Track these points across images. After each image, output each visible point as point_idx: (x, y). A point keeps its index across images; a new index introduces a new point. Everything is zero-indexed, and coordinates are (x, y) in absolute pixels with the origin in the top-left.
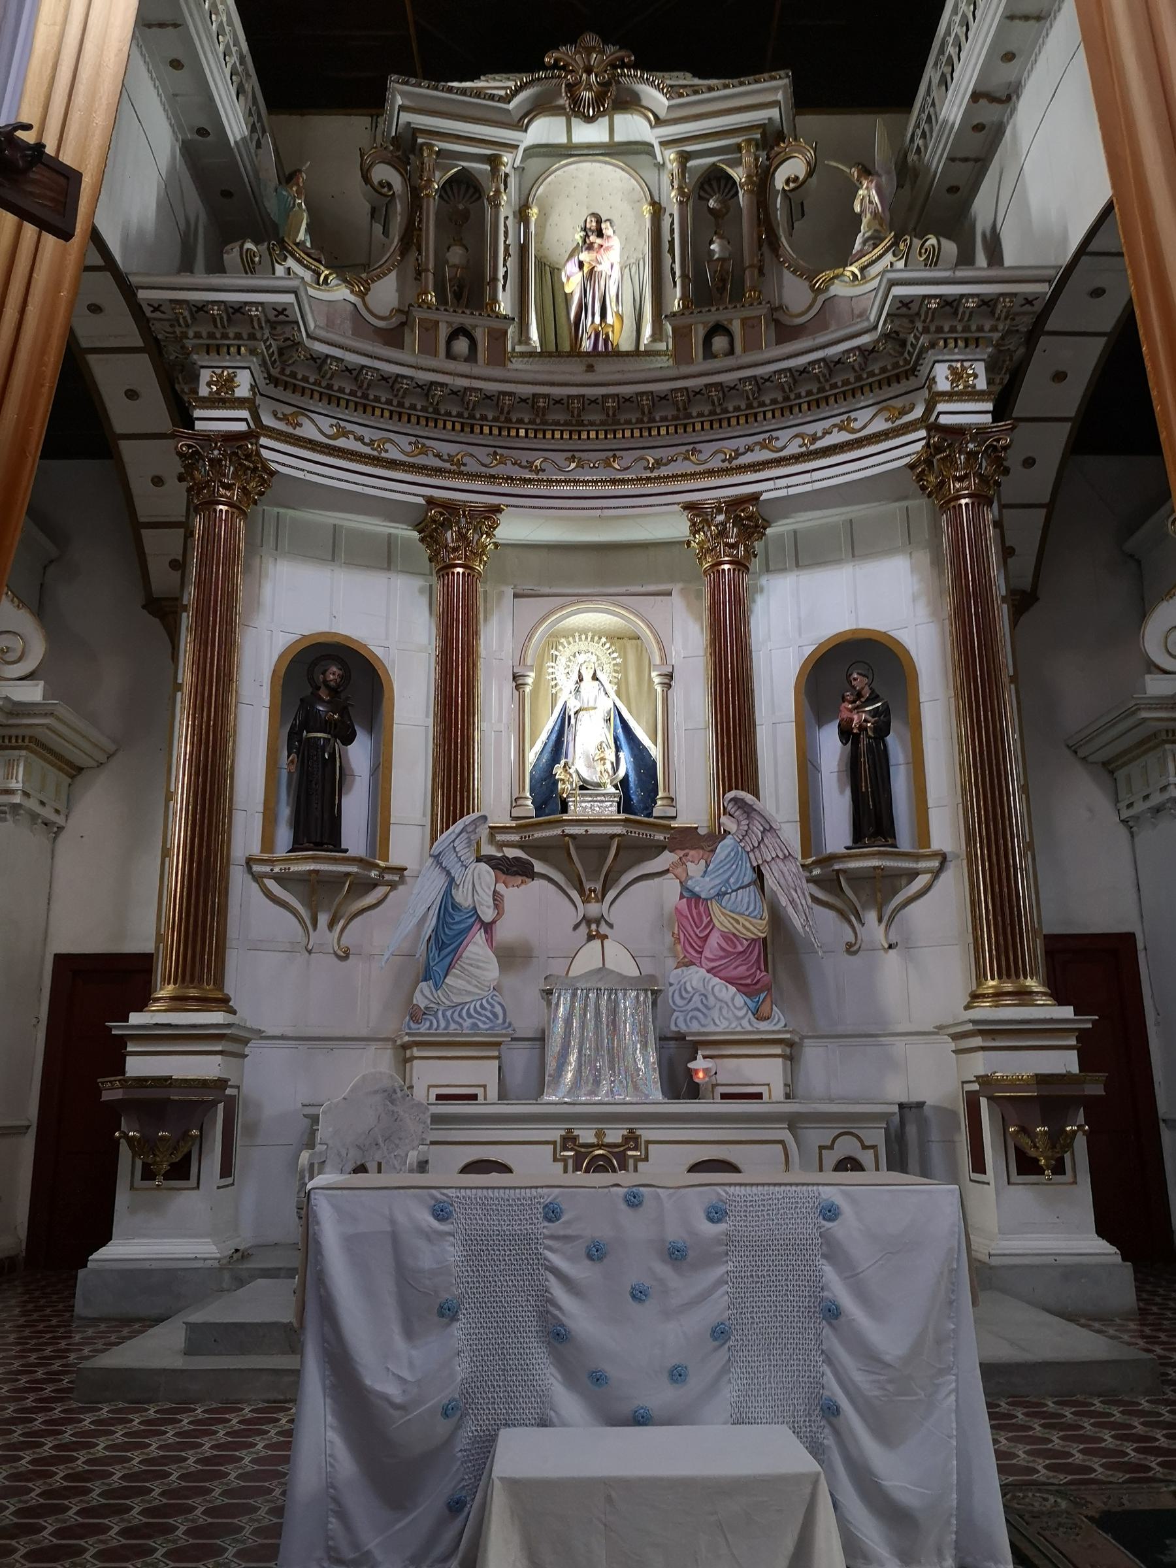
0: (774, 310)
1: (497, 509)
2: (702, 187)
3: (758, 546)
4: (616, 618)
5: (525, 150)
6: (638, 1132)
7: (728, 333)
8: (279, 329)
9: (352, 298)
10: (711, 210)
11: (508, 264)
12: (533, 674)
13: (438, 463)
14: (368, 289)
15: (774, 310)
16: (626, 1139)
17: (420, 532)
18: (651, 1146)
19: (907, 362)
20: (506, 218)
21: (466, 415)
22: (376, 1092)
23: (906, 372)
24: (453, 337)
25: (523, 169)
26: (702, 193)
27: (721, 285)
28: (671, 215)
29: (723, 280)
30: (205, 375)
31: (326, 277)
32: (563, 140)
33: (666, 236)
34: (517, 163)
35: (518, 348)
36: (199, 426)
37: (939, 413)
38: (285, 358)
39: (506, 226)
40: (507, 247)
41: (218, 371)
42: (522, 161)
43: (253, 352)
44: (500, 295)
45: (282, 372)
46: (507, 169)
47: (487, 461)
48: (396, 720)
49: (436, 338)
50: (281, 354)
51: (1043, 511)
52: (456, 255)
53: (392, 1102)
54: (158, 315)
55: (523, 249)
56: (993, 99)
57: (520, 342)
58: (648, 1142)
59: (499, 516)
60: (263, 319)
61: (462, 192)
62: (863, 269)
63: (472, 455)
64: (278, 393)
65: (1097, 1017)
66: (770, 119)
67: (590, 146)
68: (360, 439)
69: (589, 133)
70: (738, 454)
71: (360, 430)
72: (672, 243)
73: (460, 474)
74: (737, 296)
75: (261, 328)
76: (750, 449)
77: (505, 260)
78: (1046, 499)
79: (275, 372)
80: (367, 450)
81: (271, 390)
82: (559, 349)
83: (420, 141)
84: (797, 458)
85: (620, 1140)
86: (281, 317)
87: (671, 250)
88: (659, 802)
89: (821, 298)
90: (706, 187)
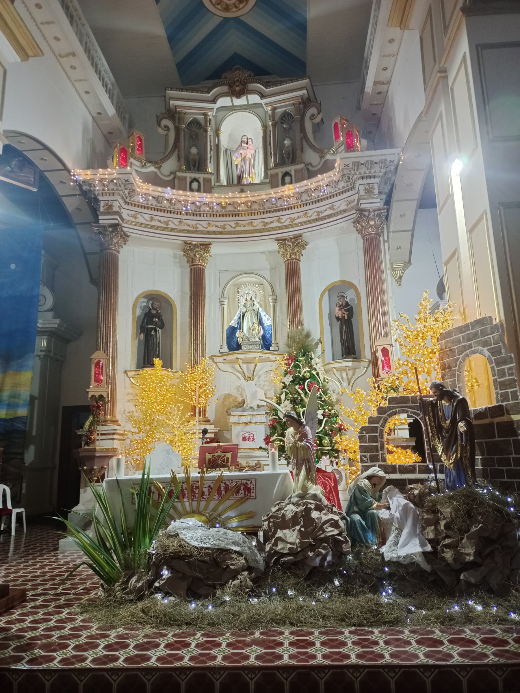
0: (307, 165)
1: (210, 244)
2: (282, 119)
3: (303, 252)
4: (255, 279)
5: (217, 109)
6: (261, 462)
7: (291, 175)
8: (127, 186)
10: (284, 128)
11: (212, 153)
12: (227, 301)
13: (188, 228)
14: (161, 166)
15: (307, 165)
16: (256, 464)
17: (184, 252)
18: (265, 467)
19: (351, 185)
20: (210, 136)
24: (191, 182)
25: (217, 116)
26: (282, 121)
27: (288, 156)
28: (270, 131)
29: (289, 155)
31: (145, 164)
32: (231, 105)
33: (268, 139)
34: (214, 114)
35: (216, 184)
36: (101, 222)
38: (130, 195)
39: (210, 139)
40: (211, 146)
42: (216, 113)
43: (119, 194)
44: (209, 165)
45: (130, 200)
46: (210, 117)
47: (206, 226)
50: (129, 194)
51: (411, 232)
52: (194, 150)
53: (168, 454)
55: (218, 146)
56: (383, 83)
57: (217, 182)
58: (264, 465)
59: (210, 246)
61: (195, 126)
64: (129, 207)
66: (303, 94)
67: (240, 106)
69: (238, 102)
72: (270, 141)
73: (196, 232)
74: (294, 162)
75: (120, 186)
76: (299, 217)
77: (210, 152)
79: (127, 200)
80: (163, 225)
83: (178, 110)
85: (254, 465)
86: (127, 182)
87: (270, 145)
88: (273, 345)
89: (323, 160)
90: (284, 118)
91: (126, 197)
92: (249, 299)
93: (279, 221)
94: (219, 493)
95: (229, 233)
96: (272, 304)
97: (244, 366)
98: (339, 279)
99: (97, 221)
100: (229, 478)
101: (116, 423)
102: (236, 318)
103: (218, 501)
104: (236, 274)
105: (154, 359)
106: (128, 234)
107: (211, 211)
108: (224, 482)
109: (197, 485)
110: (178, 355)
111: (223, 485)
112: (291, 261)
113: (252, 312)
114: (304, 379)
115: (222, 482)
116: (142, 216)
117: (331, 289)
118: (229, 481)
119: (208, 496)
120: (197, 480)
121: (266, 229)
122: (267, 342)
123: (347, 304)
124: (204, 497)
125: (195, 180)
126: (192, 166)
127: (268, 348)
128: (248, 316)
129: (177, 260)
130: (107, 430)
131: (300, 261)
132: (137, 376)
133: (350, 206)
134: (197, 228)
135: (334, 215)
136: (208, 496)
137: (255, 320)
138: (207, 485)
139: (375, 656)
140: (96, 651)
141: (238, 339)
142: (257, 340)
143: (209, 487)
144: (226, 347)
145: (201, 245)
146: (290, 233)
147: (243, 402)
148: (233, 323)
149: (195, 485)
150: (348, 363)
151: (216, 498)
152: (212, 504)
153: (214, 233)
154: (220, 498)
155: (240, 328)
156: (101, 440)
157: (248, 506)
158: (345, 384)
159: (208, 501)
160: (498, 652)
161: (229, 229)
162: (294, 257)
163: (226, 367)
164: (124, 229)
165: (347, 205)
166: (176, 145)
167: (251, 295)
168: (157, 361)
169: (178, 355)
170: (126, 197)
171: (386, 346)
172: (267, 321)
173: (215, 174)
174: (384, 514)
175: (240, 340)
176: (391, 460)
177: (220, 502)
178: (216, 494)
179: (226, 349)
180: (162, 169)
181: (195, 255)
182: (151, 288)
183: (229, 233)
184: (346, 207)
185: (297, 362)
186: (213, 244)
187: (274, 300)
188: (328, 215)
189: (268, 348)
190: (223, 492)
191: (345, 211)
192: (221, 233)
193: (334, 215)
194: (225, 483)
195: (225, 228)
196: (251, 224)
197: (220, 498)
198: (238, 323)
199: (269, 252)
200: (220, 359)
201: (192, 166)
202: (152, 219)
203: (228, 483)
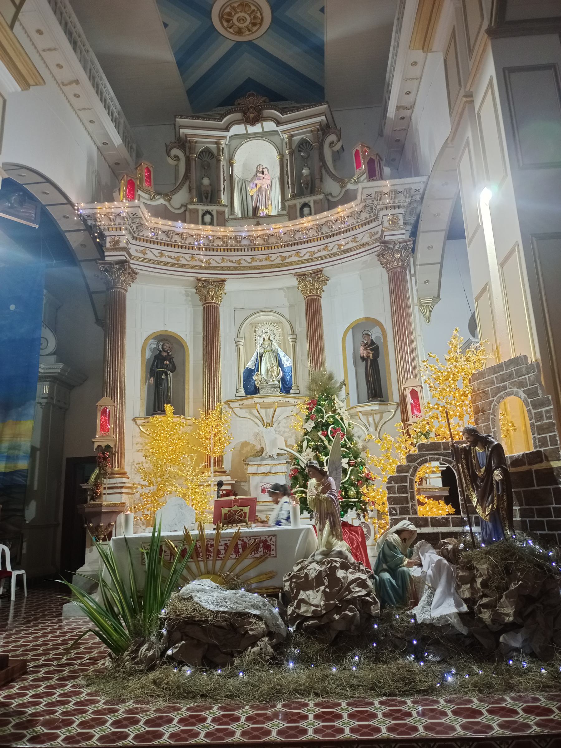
2: (299, 147)
7: (309, 206)
8: (135, 221)
9: (165, 203)
11: (225, 184)
12: (243, 341)
14: (171, 198)
20: (223, 165)
21: (211, 244)
22: (175, 505)
23: (374, 219)
24: (204, 215)
25: (230, 145)
28: (287, 160)
30: (108, 239)
31: (154, 196)
32: (245, 132)
34: (227, 143)
35: (230, 217)
36: (107, 258)
37: (385, 236)
38: (139, 229)
39: (223, 169)
40: (224, 177)
41: (113, 237)
42: (229, 142)
44: (222, 196)
48: (440, 479)
49: (198, 216)
50: (137, 228)
51: (439, 265)
54: (89, 218)
55: (231, 177)
56: (406, 108)
57: (231, 214)
59: (225, 283)
60: (128, 217)
62: (358, 179)
63: (213, 260)
64: (138, 242)
65: (35, 488)
67: (255, 134)
68: (170, 257)
69: (252, 129)
70: (314, 254)
71: (170, 254)
74: (312, 192)
76: (319, 251)
77: (224, 183)
78: (440, 261)
79: (135, 235)
80: (173, 261)
81: (134, 242)
82: (41, 357)
83: (188, 139)
84: (336, 254)
86: (135, 216)
87: (287, 174)
88: (293, 388)
89: (344, 190)
90: (301, 146)
91: (134, 232)
92: (266, 338)
93: (298, 254)
94: (236, 551)
95: (245, 268)
96: (291, 344)
97: (262, 412)
98: (363, 316)
99: (103, 257)
100: (246, 535)
101: (124, 476)
102: (253, 359)
103: (235, 560)
104: (253, 312)
105: (165, 405)
106: (137, 271)
107: (225, 245)
108: (242, 539)
109: (212, 543)
110: (191, 400)
111: (240, 542)
112: (312, 297)
113: (271, 353)
114: (327, 425)
115: (240, 540)
116: (151, 252)
117: (355, 327)
118: (246, 537)
119: (224, 555)
120: (212, 537)
121: (284, 263)
122: (287, 385)
123: (373, 343)
124: (220, 556)
125: (208, 212)
126: (204, 197)
127: (288, 392)
128: (266, 357)
129: (189, 298)
130: (114, 484)
131: (321, 297)
132: (146, 424)
133: (373, 238)
134: (211, 263)
135: (357, 248)
136: (224, 555)
137: (274, 362)
138: (223, 543)
139: (471, 728)
140: (103, 727)
141: (256, 382)
142: (276, 382)
143: (226, 544)
144: (243, 390)
145: (214, 281)
146: (309, 268)
147: (262, 450)
148: (250, 365)
149: (209, 543)
150: (375, 406)
151: (233, 557)
152: (229, 563)
153: (229, 268)
154: (237, 557)
155: (258, 370)
156: (108, 494)
157: (268, 565)
158: (372, 429)
159: (225, 560)
160: (487, 731)
161: (244, 264)
162: (314, 293)
163: (243, 413)
164: (132, 266)
165: (371, 238)
166: (187, 176)
167: (269, 334)
168: (168, 408)
169: (191, 400)
170: (134, 232)
171: (415, 388)
172: (287, 362)
173: (229, 206)
174: (415, 572)
175: (257, 383)
176: (422, 512)
177: (238, 561)
178: (233, 552)
179: (242, 393)
180: (171, 202)
181: (208, 293)
182: (161, 328)
183: (245, 268)
184: (369, 239)
185: (319, 407)
186: (228, 281)
187: (294, 340)
188: (350, 249)
189: (288, 392)
190: (241, 550)
191: (368, 244)
192: (236, 268)
193: (357, 248)
194: (243, 541)
195: (240, 264)
196: (268, 258)
197: (237, 557)
198: (255, 365)
199: (288, 288)
200: (236, 404)
201: (204, 197)
202: (162, 255)
203: (246, 540)
